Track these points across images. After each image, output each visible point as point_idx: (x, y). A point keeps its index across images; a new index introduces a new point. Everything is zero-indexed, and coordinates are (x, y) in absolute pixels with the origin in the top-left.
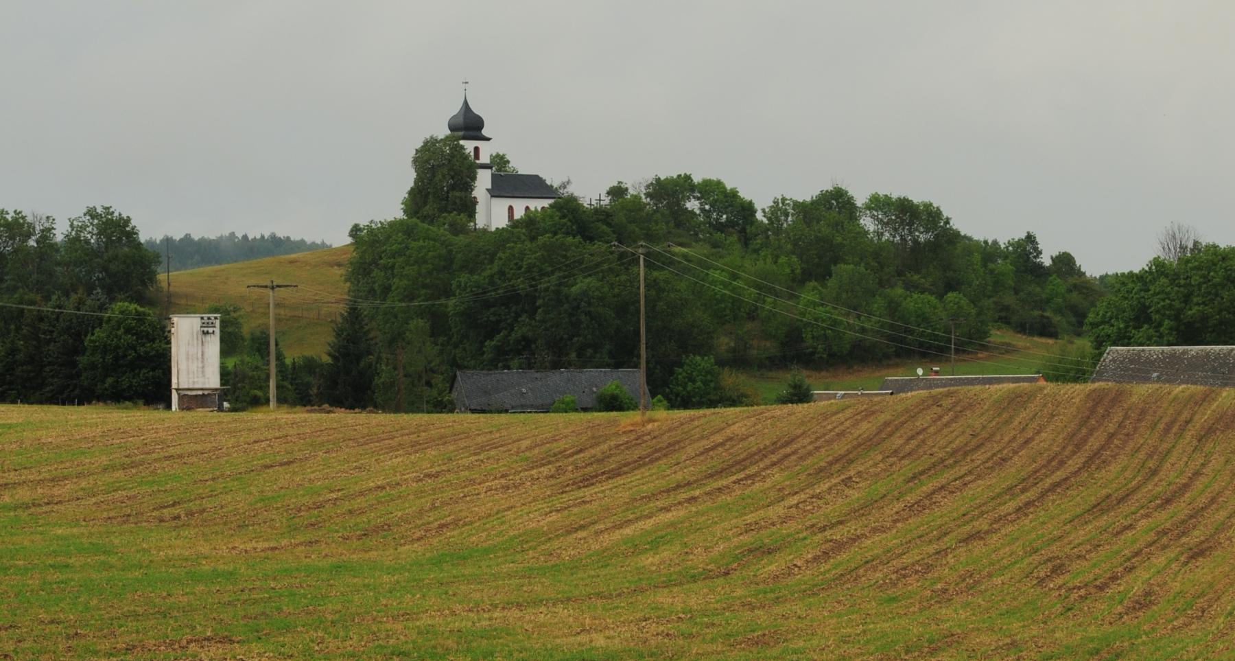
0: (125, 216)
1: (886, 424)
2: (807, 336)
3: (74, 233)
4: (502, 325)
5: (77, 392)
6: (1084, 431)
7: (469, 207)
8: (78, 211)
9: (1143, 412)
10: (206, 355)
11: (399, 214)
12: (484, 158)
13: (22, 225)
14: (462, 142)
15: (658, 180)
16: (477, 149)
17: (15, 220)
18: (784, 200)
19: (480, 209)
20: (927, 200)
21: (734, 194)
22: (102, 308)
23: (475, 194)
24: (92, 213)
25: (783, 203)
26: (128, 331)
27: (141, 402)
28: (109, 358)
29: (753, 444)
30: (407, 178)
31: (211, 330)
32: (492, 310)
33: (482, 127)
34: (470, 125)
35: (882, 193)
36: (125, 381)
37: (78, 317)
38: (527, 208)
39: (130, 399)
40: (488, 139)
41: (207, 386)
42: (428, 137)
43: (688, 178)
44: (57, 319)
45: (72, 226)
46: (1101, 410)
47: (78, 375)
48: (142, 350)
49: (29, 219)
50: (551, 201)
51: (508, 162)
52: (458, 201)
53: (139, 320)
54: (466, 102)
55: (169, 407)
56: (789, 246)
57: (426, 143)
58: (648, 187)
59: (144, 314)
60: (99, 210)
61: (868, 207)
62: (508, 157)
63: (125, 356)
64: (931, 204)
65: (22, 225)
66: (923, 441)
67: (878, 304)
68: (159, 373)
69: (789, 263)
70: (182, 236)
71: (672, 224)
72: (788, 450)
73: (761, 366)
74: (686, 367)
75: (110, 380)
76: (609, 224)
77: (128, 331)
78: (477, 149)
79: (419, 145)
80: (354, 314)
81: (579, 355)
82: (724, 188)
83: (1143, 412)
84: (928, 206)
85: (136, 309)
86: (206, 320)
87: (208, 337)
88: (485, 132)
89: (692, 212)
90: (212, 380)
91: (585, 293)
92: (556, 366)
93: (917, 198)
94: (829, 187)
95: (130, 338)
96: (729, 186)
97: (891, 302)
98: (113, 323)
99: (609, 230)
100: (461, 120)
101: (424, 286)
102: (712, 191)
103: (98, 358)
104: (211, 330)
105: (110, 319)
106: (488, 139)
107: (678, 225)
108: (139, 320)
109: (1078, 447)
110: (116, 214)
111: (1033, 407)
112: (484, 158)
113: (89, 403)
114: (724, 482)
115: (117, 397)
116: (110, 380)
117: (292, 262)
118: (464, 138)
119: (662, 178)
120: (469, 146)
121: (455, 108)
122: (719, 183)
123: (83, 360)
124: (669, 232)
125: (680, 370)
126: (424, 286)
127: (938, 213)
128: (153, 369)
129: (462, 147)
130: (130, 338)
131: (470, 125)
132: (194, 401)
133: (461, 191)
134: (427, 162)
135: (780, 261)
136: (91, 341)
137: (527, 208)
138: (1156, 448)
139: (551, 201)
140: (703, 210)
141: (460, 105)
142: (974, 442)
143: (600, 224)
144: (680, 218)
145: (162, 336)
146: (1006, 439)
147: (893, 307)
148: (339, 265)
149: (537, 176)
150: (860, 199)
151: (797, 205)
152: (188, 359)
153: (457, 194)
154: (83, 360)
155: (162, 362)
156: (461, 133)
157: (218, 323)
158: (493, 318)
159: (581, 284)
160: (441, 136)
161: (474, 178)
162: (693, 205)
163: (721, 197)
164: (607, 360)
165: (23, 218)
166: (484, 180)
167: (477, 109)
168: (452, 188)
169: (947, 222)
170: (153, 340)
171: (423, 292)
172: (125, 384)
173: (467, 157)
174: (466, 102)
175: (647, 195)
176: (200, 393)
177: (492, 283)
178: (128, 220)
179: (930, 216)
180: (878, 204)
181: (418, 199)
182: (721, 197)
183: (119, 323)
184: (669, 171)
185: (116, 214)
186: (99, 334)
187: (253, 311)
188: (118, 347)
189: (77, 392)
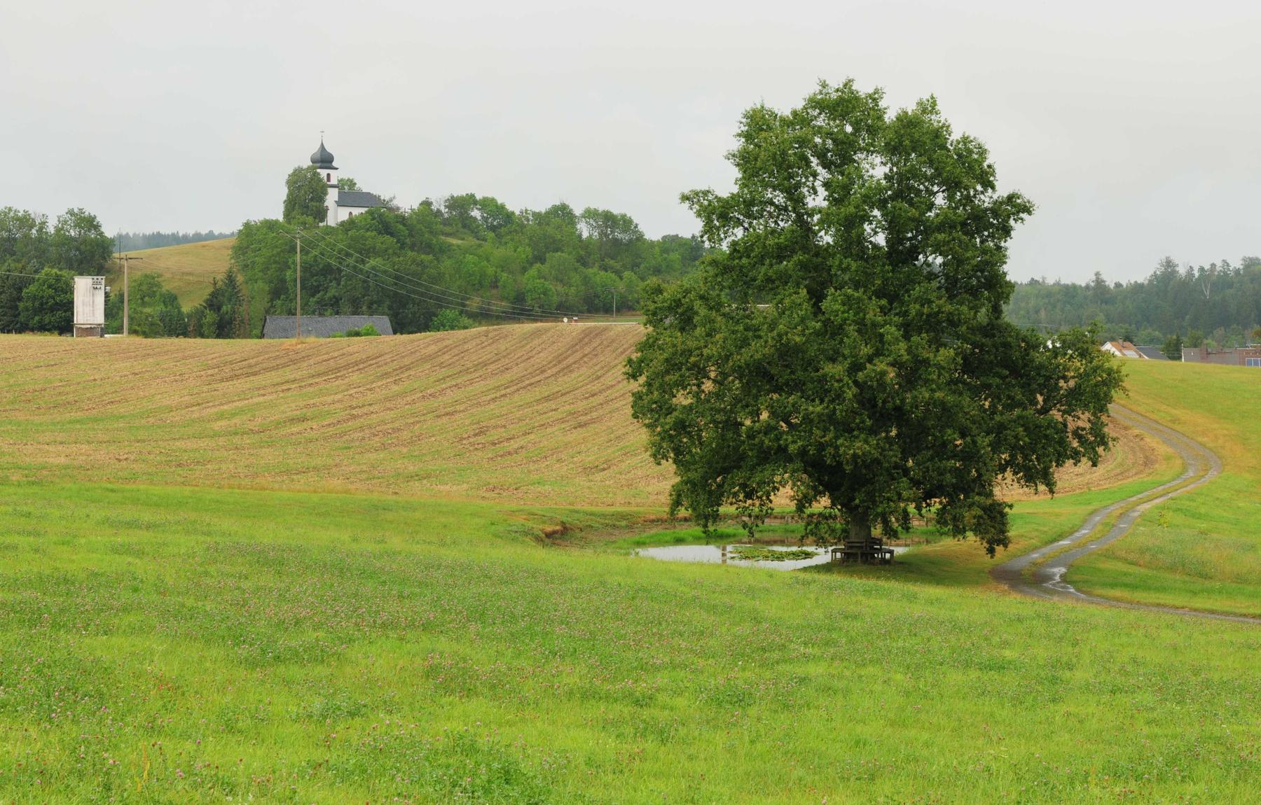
0: (92, 214)
1: (446, 347)
2: (528, 298)
3: (60, 225)
4: (321, 288)
5: (18, 325)
6: (569, 352)
7: (321, 214)
8: (62, 211)
9: (613, 341)
10: (96, 302)
11: (277, 213)
12: (334, 181)
13: (28, 220)
14: (318, 170)
15: (452, 197)
16: (329, 175)
17: (25, 217)
18: (526, 210)
19: (330, 214)
20: (623, 212)
21: (502, 207)
22: (36, 272)
23: (326, 204)
24: (71, 213)
25: (526, 213)
26: (50, 287)
27: (56, 332)
28: (37, 304)
29: (356, 357)
30: (283, 193)
31: (98, 287)
32: (315, 278)
33: (333, 161)
34: (325, 160)
35: (592, 207)
36: (47, 319)
37: (20, 277)
38: (351, 213)
39: (49, 330)
40: (337, 169)
41: (96, 322)
42: (297, 166)
43: (473, 196)
44: (8, 278)
45: (59, 221)
46: (586, 340)
47: (19, 314)
48: (58, 299)
49: (33, 216)
50: (366, 209)
51: (355, 184)
52: (314, 208)
53: (57, 280)
54: (322, 144)
55: (73, 336)
56: (527, 241)
57: (295, 171)
58: (446, 201)
59: (61, 276)
60: (76, 211)
61: (583, 216)
62: (355, 181)
63: (47, 303)
64: (625, 215)
65: (28, 220)
66: (463, 358)
67: (576, 278)
68: (68, 314)
69: (525, 251)
70: (207, 232)
71: (460, 225)
72: (374, 361)
73: (498, 317)
74: (439, 317)
75: (37, 318)
76: (404, 225)
77: (50, 287)
78: (329, 175)
79: (291, 171)
80: (230, 279)
81: (369, 308)
82: (497, 203)
83: (613, 341)
84: (624, 216)
85: (56, 273)
86: (95, 280)
87: (97, 291)
88: (334, 164)
89: (475, 219)
90: (99, 318)
91: (373, 268)
92: (354, 313)
93: (616, 211)
94: (558, 203)
95: (51, 291)
96: (499, 202)
97: (586, 277)
98: (41, 281)
99: (404, 228)
100: (318, 156)
101: (275, 262)
102: (489, 205)
103: (30, 304)
104: (98, 287)
105: (39, 279)
106: (337, 169)
107: (464, 226)
108: (57, 280)
109: (559, 362)
110: (87, 213)
111: (549, 334)
112: (334, 181)
113: (25, 332)
114: (317, 380)
115: (43, 328)
116: (37, 318)
117: (204, 246)
118: (321, 168)
119: (455, 196)
120: (323, 173)
121: (315, 148)
122: (493, 200)
123: (21, 305)
124: (458, 231)
125: (436, 319)
126: (275, 262)
127: (630, 221)
128: (65, 312)
129: (319, 174)
130: (51, 291)
131: (325, 160)
132: (89, 331)
133: (317, 201)
134: (295, 183)
135: (519, 250)
136: (26, 293)
137: (351, 213)
138: (609, 363)
139: (366, 209)
140: (483, 217)
141: (318, 146)
142: (496, 358)
143: (398, 224)
144: (467, 223)
145: (69, 290)
146: (516, 357)
147: (586, 280)
148: (228, 249)
149: (369, 193)
150: (578, 211)
151: (534, 214)
152: (83, 305)
153: (315, 204)
154: (21, 305)
155: (69, 306)
156: (319, 165)
157: (103, 281)
158: (315, 284)
159: (373, 262)
160: (305, 167)
161: (326, 194)
162: (476, 213)
163: (494, 208)
164: (386, 310)
165: (29, 215)
166: (332, 196)
167: (329, 149)
168: (312, 200)
169: (636, 227)
170: (66, 293)
171: (274, 266)
172: (47, 321)
173: (320, 180)
174: (322, 144)
175: (446, 207)
176: (89, 326)
177: (315, 261)
178: (95, 217)
179: (626, 223)
180: (590, 214)
181: (292, 205)
182: (494, 208)
183: (44, 282)
184: (460, 192)
185: (87, 213)
186: (32, 288)
187: (173, 278)
188: (43, 297)
189: (18, 325)
